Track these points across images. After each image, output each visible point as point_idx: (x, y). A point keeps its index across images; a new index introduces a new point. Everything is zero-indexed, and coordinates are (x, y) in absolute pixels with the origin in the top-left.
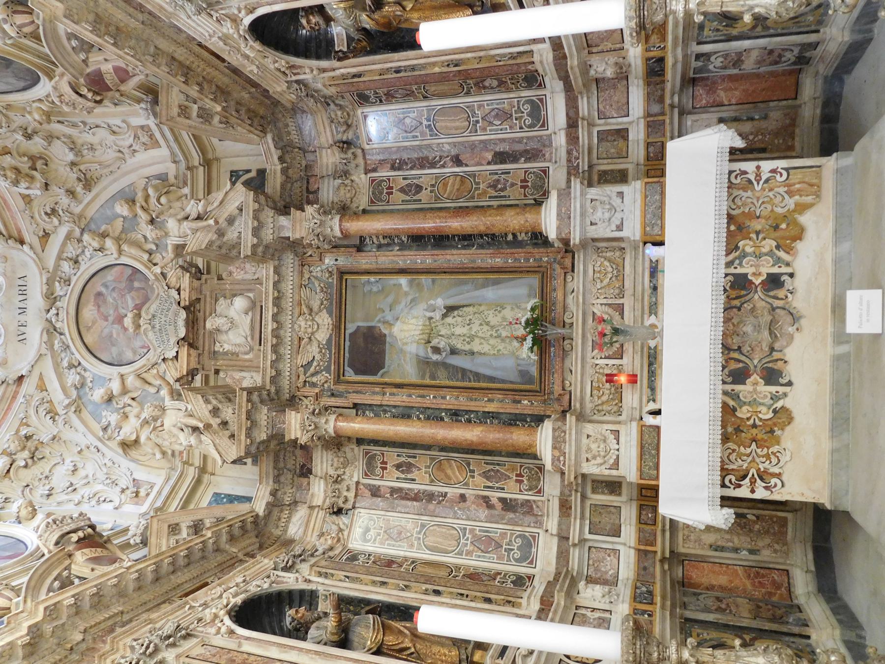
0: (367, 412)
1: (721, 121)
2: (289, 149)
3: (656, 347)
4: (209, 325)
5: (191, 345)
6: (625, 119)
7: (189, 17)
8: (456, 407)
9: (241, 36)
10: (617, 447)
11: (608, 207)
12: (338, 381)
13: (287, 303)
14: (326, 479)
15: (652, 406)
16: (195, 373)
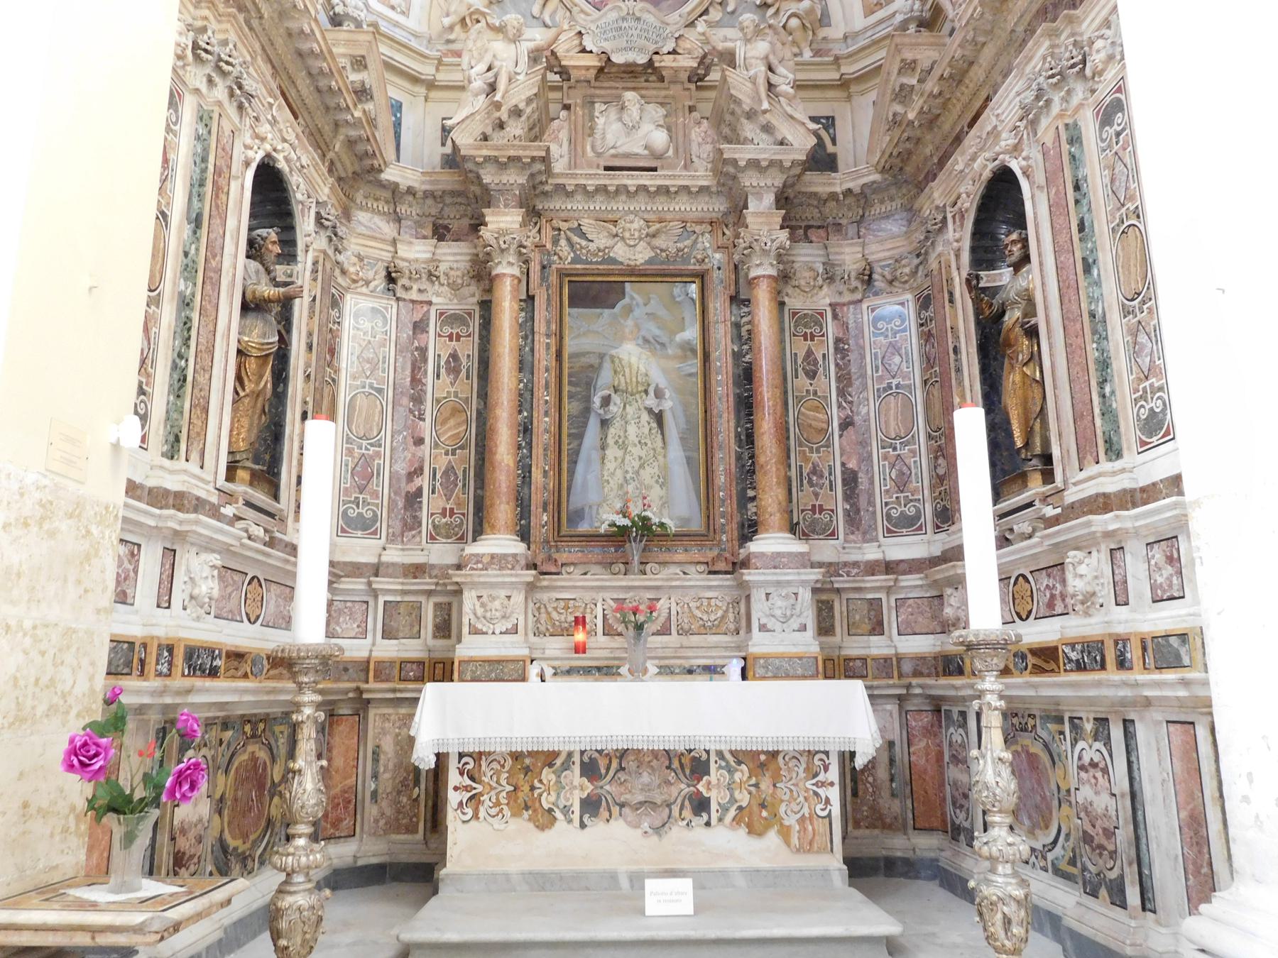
0: (523, 314)
1: (891, 744)
2: (862, 202)
3: (619, 674)
4: (630, 96)
5: (601, 70)
6: (895, 631)
7: (1018, 94)
8: (535, 430)
9: (998, 154)
10: (497, 632)
11: (788, 613)
12: (562, 274)
13: (661, 204)
14: (433, 260)
15: (549, 672)
16: (565, 77)
